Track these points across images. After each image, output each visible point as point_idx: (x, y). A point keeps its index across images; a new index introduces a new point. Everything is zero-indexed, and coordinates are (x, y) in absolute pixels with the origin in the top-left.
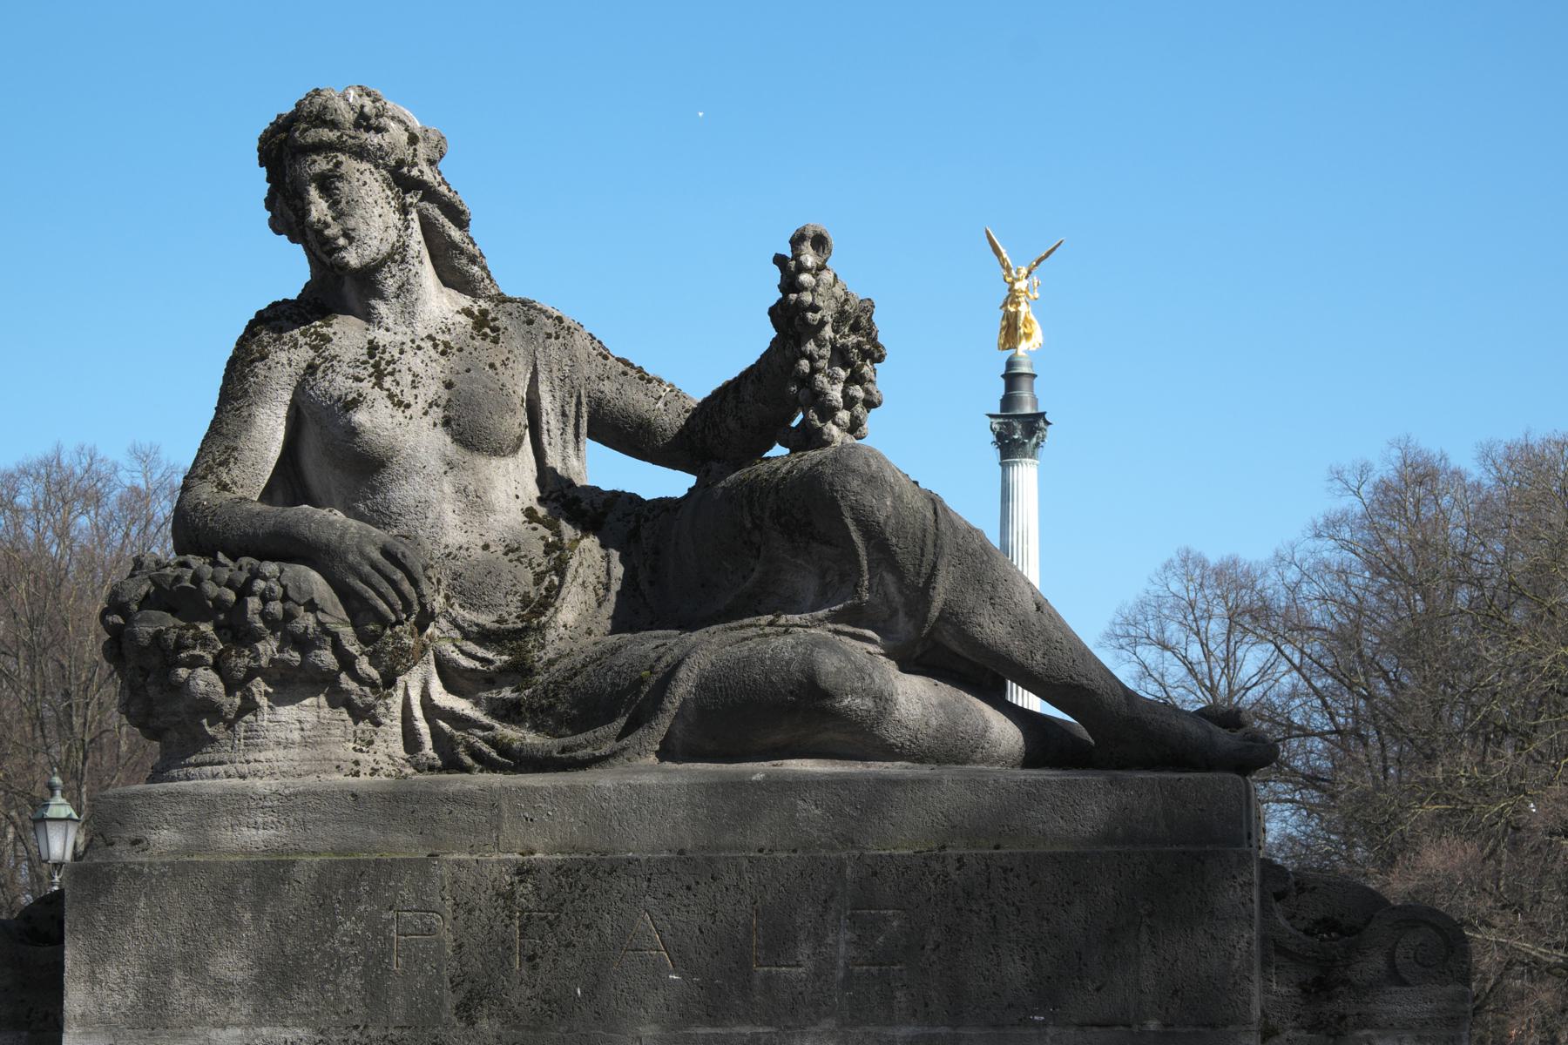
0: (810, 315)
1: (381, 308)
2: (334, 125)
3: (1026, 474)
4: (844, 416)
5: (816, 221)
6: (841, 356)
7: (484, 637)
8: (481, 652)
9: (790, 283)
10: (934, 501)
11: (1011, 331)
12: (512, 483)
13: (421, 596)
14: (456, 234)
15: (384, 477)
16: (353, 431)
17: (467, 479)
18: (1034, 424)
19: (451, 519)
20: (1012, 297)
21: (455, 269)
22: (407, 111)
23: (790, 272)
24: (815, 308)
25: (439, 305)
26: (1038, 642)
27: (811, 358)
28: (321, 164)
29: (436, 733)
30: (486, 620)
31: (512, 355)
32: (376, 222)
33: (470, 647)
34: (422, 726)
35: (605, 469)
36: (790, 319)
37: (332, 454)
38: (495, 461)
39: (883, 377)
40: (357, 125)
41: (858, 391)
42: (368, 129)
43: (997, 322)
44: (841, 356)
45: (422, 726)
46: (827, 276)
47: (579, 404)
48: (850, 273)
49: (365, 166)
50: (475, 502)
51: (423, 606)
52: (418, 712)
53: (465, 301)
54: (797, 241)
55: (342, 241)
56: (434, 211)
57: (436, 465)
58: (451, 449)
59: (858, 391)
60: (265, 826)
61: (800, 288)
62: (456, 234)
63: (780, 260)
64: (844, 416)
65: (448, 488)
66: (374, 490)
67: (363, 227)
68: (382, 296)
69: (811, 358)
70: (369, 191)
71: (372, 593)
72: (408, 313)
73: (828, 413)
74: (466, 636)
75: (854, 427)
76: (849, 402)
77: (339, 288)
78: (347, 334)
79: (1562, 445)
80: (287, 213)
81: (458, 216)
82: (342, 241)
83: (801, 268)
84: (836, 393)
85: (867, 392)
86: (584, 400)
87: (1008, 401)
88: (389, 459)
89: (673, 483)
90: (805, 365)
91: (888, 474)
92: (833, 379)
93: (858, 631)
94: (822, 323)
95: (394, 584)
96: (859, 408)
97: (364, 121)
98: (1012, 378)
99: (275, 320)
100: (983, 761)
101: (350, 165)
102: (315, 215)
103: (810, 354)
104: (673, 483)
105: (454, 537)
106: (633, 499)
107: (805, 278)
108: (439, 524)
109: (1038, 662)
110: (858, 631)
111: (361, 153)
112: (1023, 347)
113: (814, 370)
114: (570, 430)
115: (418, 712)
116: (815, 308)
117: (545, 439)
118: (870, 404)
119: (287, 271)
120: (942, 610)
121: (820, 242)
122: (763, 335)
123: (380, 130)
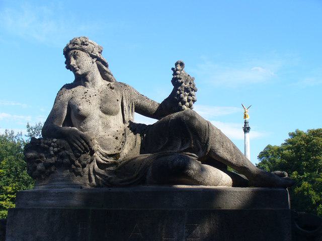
0: (179, 80)
1: (88, 84)
2: (77, 44)
3: (247, 134)
4: (188, 104)
5: (184, 62)
6: (187, 90)
7: (110, 156)
8: (106, 160)
9: (175, 74)
10: (208, 123)
11: (245, 116)
12: (116, 123)
13: (89, 146)
14: (105, 68)
15: (86, 120)
16: (79, 110)
17: (105, 120)
18: (248, 128)
19: (101, 128)
20: (245, 112)
21: (105, 75)
22: (94, 43)
23: (175, 71)
24: (180, 79)
25: (101, 83)
26: (234, 156)
27: (180, 90)
28: (72, 52)
29: (96, 178)
30: (108, 152)
31: (118, 96)
32: (86, 64)
33: (104, 158)
34: (93, 177)
35: (140, 119)
36: (176, 82)
37: (75, 116)
38: (111, 116)
39: (197, 95)
40: (82, 44)
41: (191, 98)
42: (84, 45)
43: (243, 115)
44: (187, 90)
45: (93, 177)
46: (182, 71)
47: (132, 104)
48: (188, 70)
49: (83, 53)
50: (106, 126)
51: (91, 149)
52: (92, 173)
53: (108, 83)
54: (176, 64)
55: (77, 69)
56: (100, 63)
57: (97, 117)
58: (101, 114)
59: (191, 98)
60: (52, 200)
61: (177, 74)
62: (105, 68)
63: (173, 69)
64: (188, 104)
65: (100, 123)
66: (84, 123)
67: (82, 66)
68: (88, 81)
69: (180, 90)
70: (83, 56)
71: (77, 146)
72: (94, 84)
73: (184, 103)
74: (103, 156)
75: (190, 106)
76: (189, 100)
77: (82, 80)
78: (80, 89)
79: (316, 133)
80: (69, 66)
81: (106, 66)
82: (77, 69)
83: (177, 70)
84: (186, 99)
85: (193, 98)
86: (134, 104)
87: (245, 126)
88: (89, 115)
89: (150, 121)
90: (178, 92)
91: (197, 116)
92: (185, 95)
93: (191, 154)
94: (182, 82)
95: (82, 144)
96: (191, 102)
97: (83, 43)
98: (245, 123)
99: (68, 87)
100: (221, 185)
101: (81, 53)
102: (72, 63)
103: (181, 90)
104: (150, 121)
105: (102, 133)
106: (144, 125)
107: (178, 72)
108: (98, 130)
109: (234, 161)
110: (191, 154)
111: (83, 50)
112: (247, 119)
113: (181, 93)
114: (130, 110)
115: (92, 173)
116: (180, 79)
117: (124, 112)
118: (194, 101)
119: (70, 78)
120: (211, 149)
121: (182, 64)
122: (171, 87)
123: (87, 45)
